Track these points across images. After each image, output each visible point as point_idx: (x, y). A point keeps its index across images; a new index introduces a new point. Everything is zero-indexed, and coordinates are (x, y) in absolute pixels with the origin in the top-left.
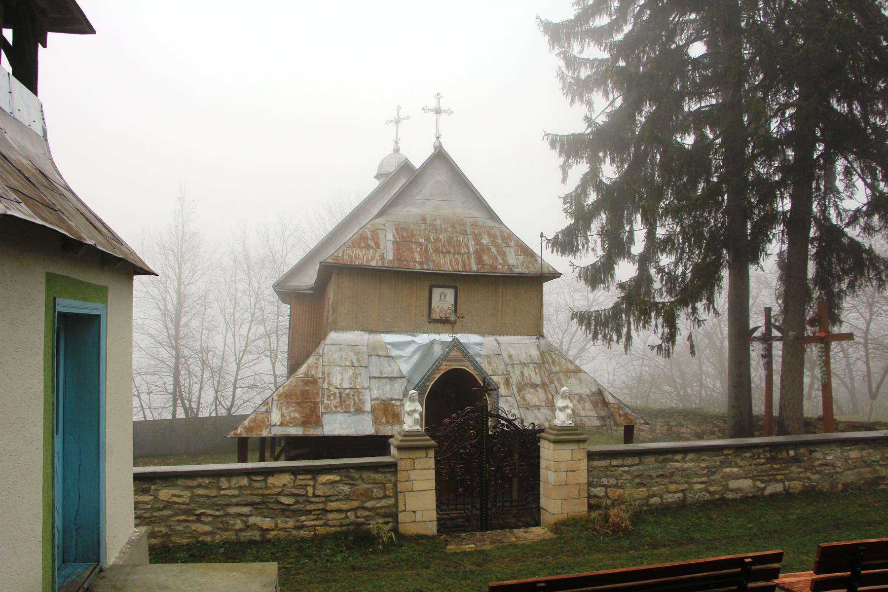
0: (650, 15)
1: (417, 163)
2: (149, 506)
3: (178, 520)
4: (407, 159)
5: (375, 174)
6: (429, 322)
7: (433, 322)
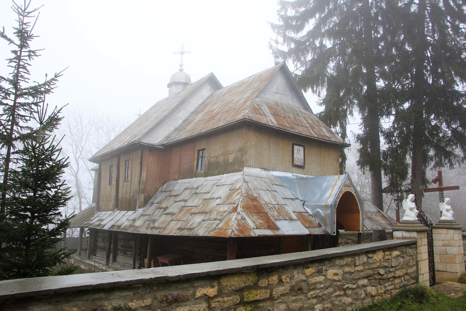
0: (451, 5)
1: (194, 79)
2: (322, 286)
3: (336, 296)
4: (213, 73)
5: (168, 82)
6: (293, 166)
7: (295, 166)
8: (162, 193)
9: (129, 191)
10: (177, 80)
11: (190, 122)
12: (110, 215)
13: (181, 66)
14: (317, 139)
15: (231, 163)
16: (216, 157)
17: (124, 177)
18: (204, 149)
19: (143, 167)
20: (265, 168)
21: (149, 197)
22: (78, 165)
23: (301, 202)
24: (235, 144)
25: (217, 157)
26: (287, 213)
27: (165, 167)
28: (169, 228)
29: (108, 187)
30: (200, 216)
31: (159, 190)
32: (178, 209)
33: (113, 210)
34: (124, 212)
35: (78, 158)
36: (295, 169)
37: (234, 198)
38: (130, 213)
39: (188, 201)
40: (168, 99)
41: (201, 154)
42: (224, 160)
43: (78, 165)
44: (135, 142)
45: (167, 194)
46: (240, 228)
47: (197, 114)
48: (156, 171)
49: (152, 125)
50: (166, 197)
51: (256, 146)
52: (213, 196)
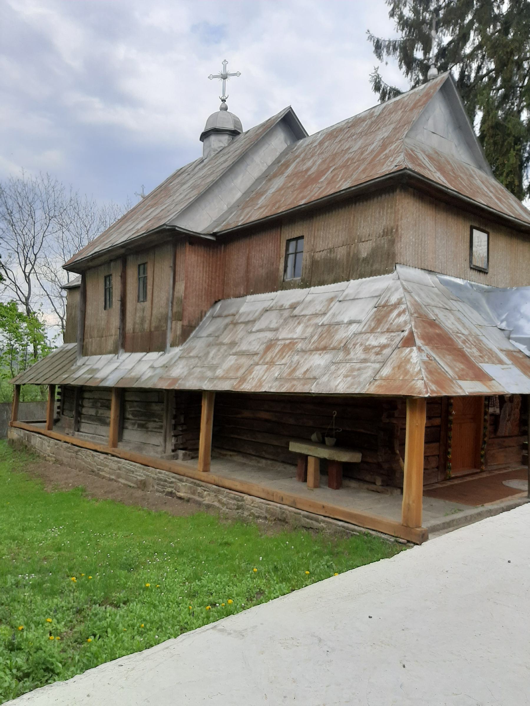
4: (291, 108)
6: (471, 268)
8: (213, 321)
9: (149, 318)
10: (219, 126)
11: (260, 194)
12: (110, 362)
13: (224, 101)
14: (514, 219)
15: (364, 260)
16: (329, 250)
17: (137, 294)
18: (302, 237)
19: (177, 273)
20: (430, 269)
21: (191, 327)
22: (29, 283)
23: (502, 333)
24: (375, 224)
25: (331, 250)
26: (490, 351)
27: (217, 274)
28: (253, 378)
29: (103, 314)
30: (320, 355)
31: (207, 315)
32: (262, 344)
33: (115, 351)
34: (138, 356)
35: (30, 273)
36: (474, 274)
37: (394, 321)
38: (153, 355)
39: (280, 329)
40: (203, 161)
41: (291, 250)
42: (349, 254)
43: (29, 283)
44: (165, 227)
45: (228, 320)
46: (435, 378)
47: (270, 180)
48: (201, 281)
49: (191, 198)
50: (227, 325)
51: (416, 225)
52: (339, 319)
